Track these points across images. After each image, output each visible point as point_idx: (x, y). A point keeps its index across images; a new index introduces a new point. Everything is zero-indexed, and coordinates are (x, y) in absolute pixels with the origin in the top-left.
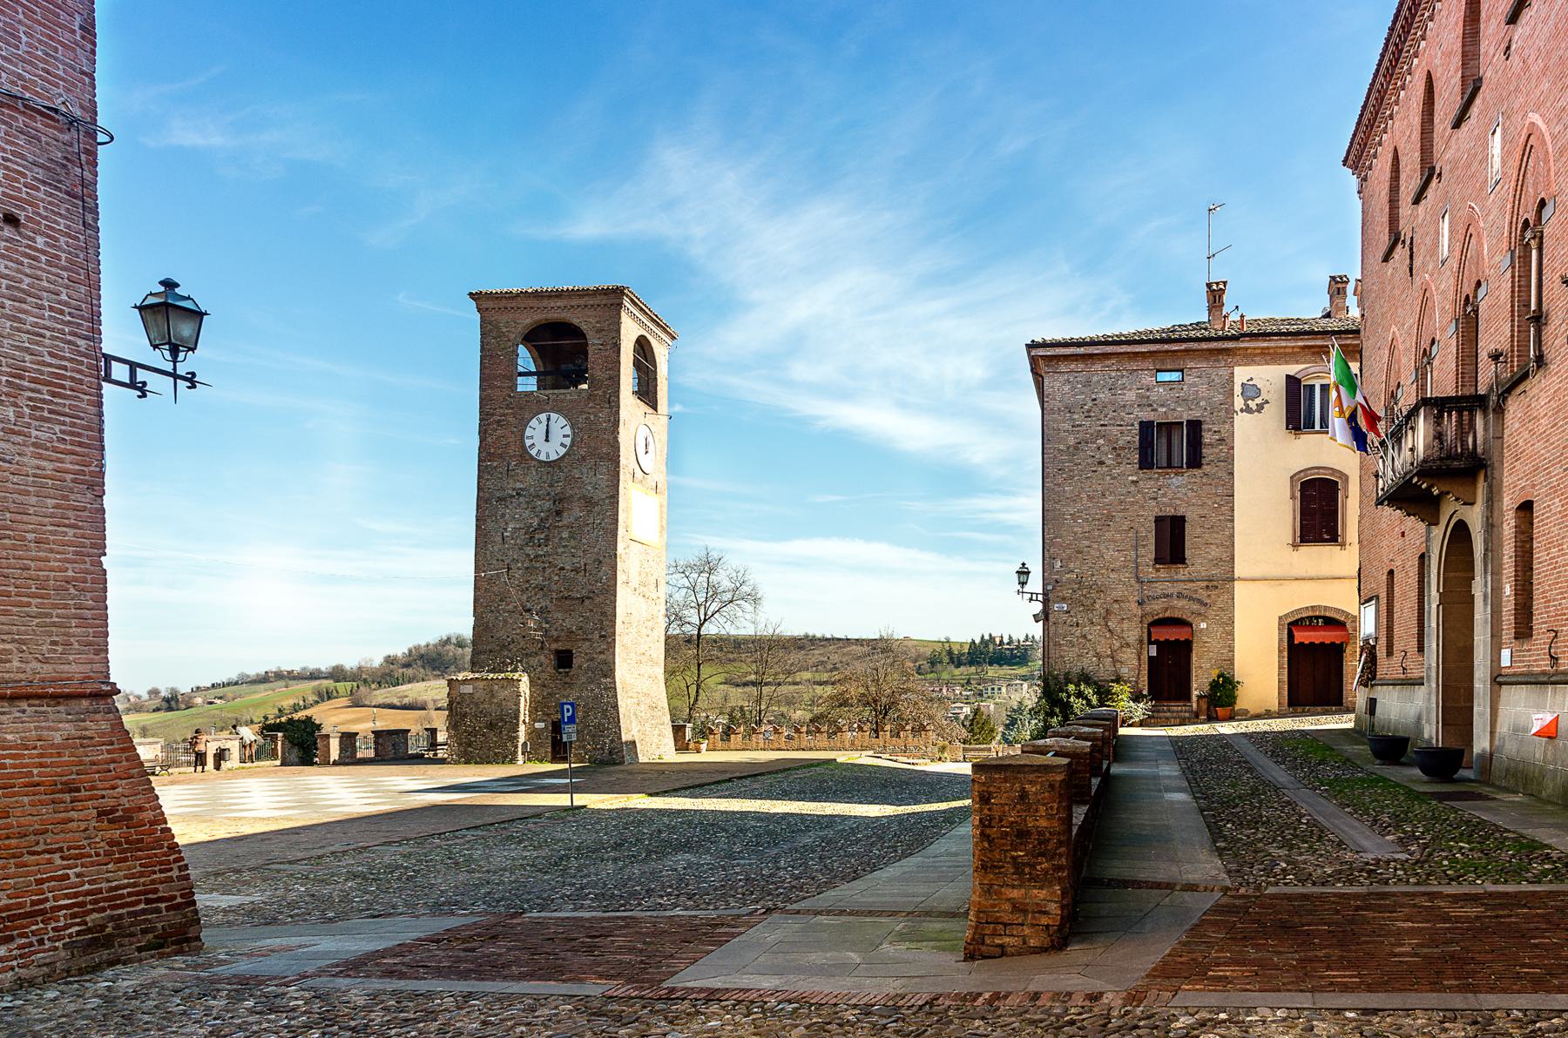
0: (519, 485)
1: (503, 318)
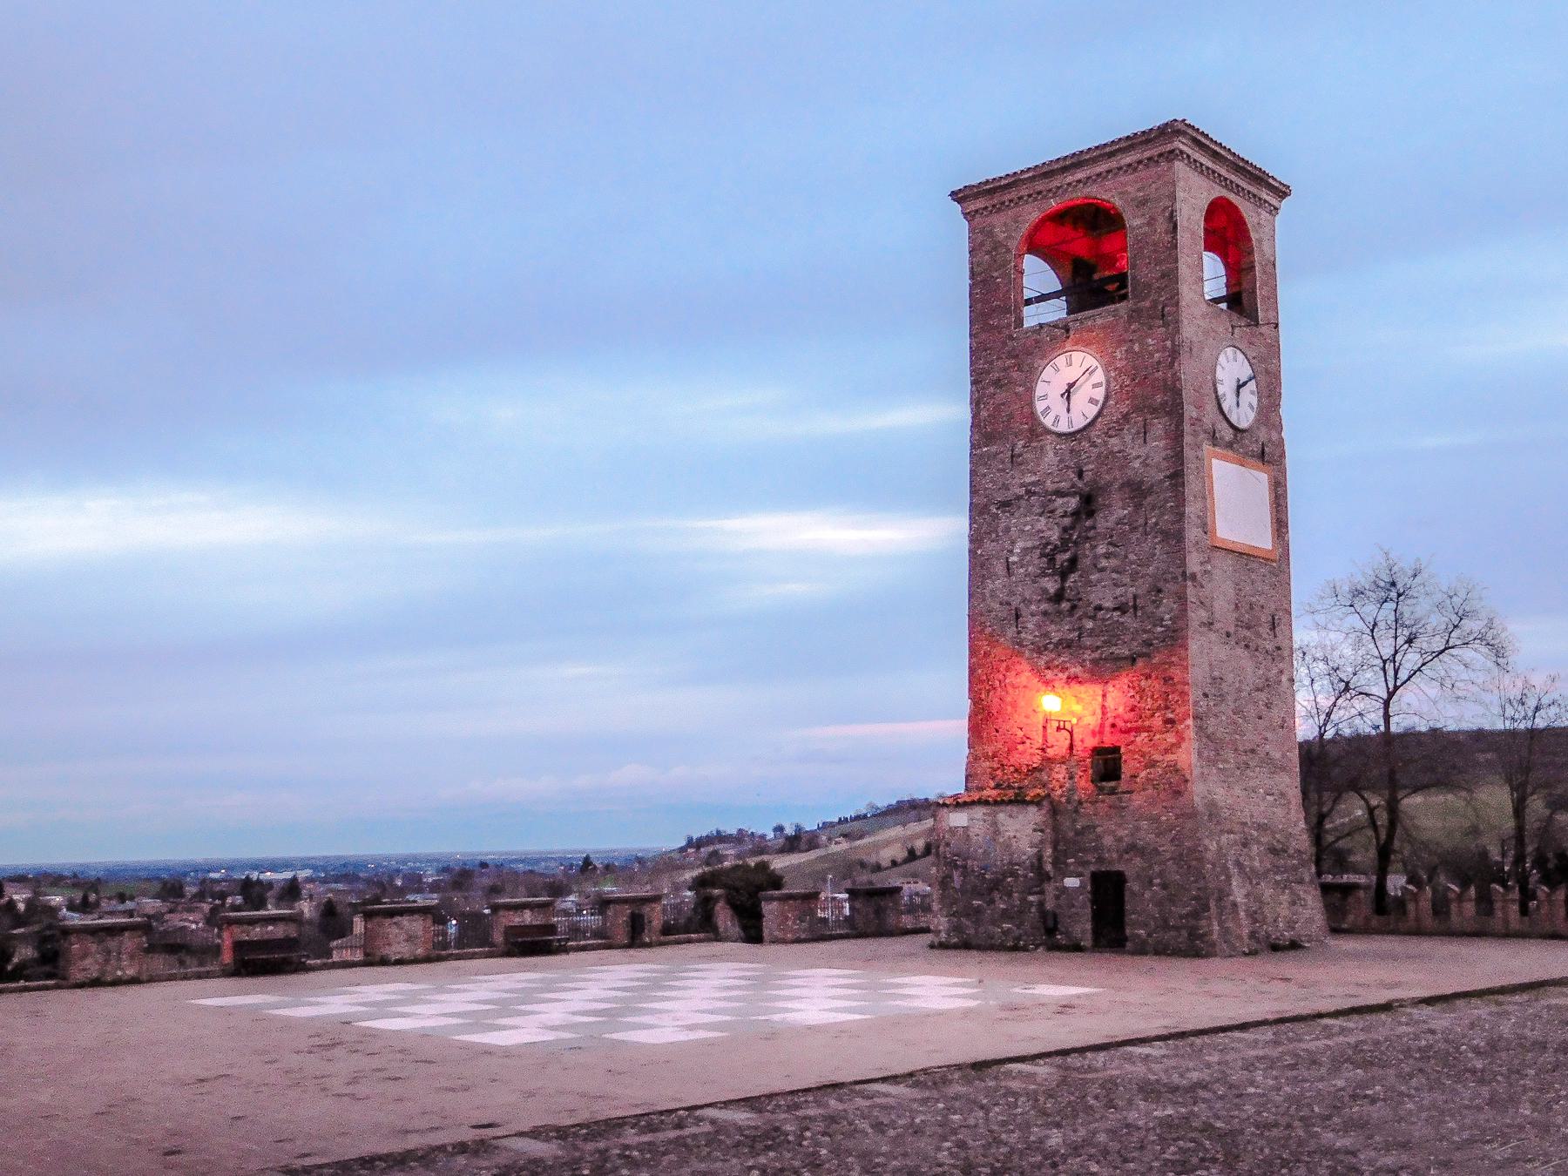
0: (1029, 479)
1: (998, 222)
